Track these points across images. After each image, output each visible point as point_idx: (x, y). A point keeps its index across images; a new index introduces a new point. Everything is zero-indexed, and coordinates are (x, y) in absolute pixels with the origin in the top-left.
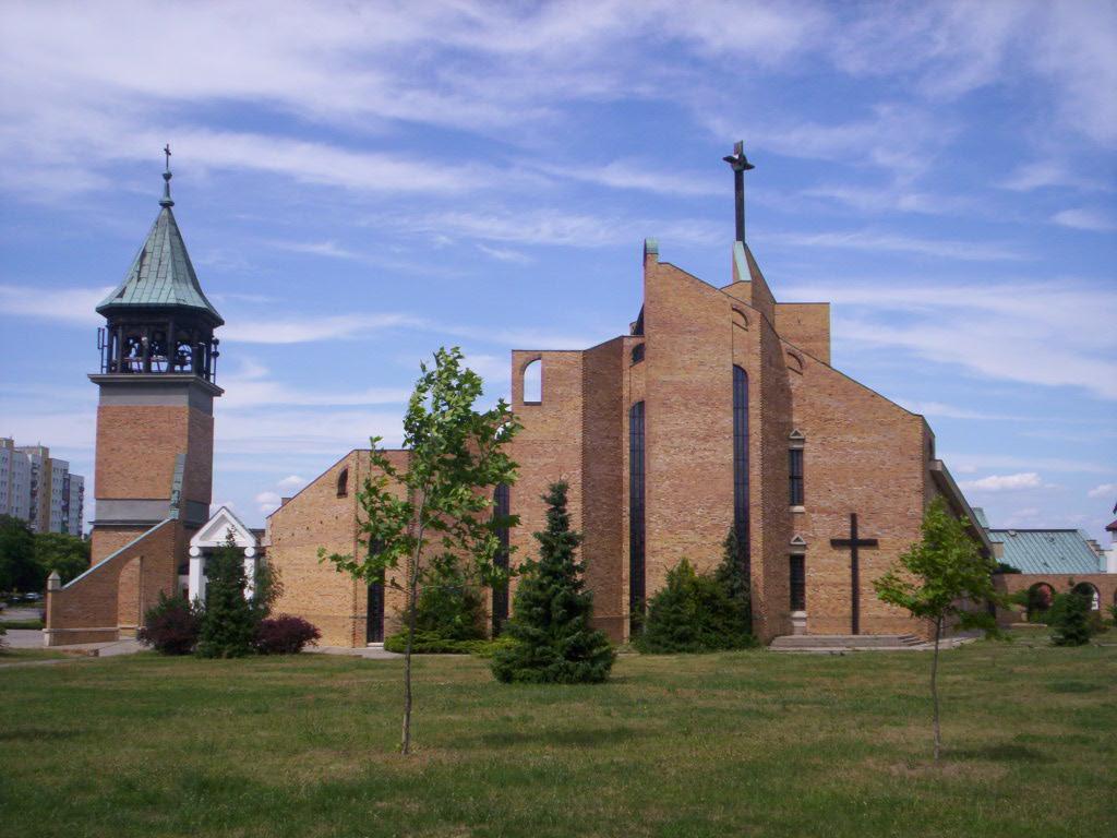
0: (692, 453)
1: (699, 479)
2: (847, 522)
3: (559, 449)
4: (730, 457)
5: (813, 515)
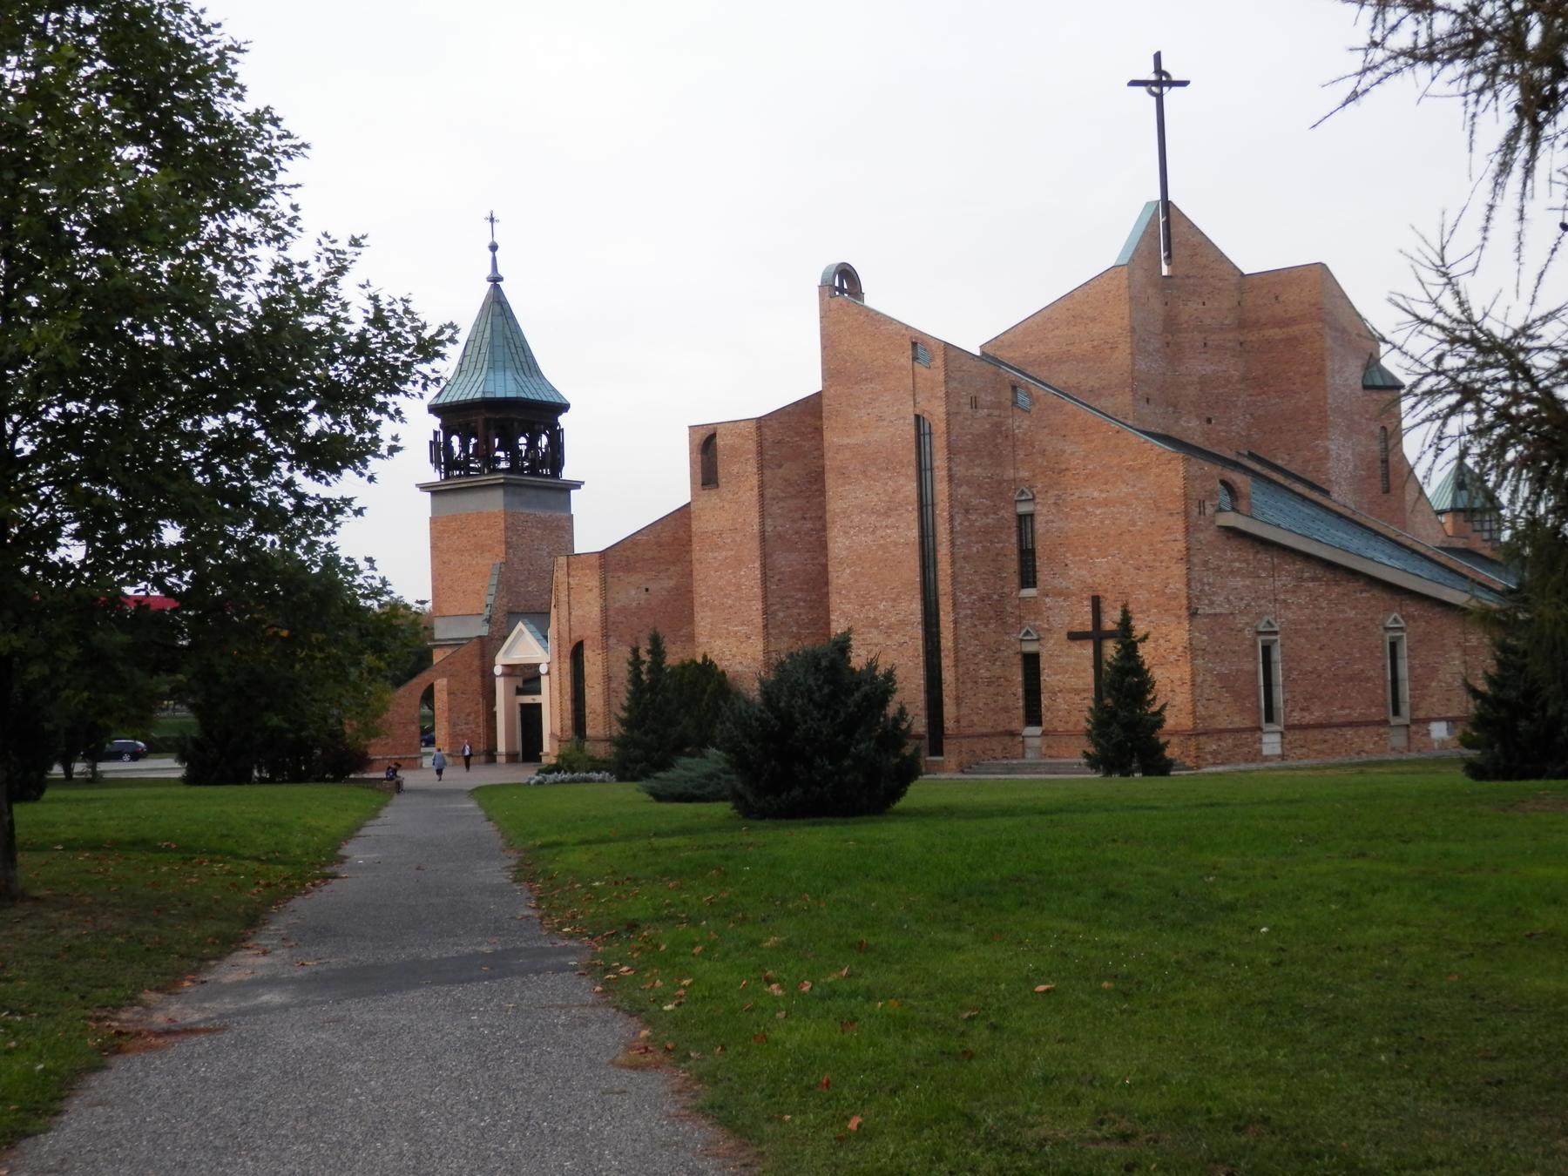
0: (873, 532)
1: (881, 565)
2: (1087, 608)
3: (738, 539)
4: (914, 534)
5: (1047, 600)
